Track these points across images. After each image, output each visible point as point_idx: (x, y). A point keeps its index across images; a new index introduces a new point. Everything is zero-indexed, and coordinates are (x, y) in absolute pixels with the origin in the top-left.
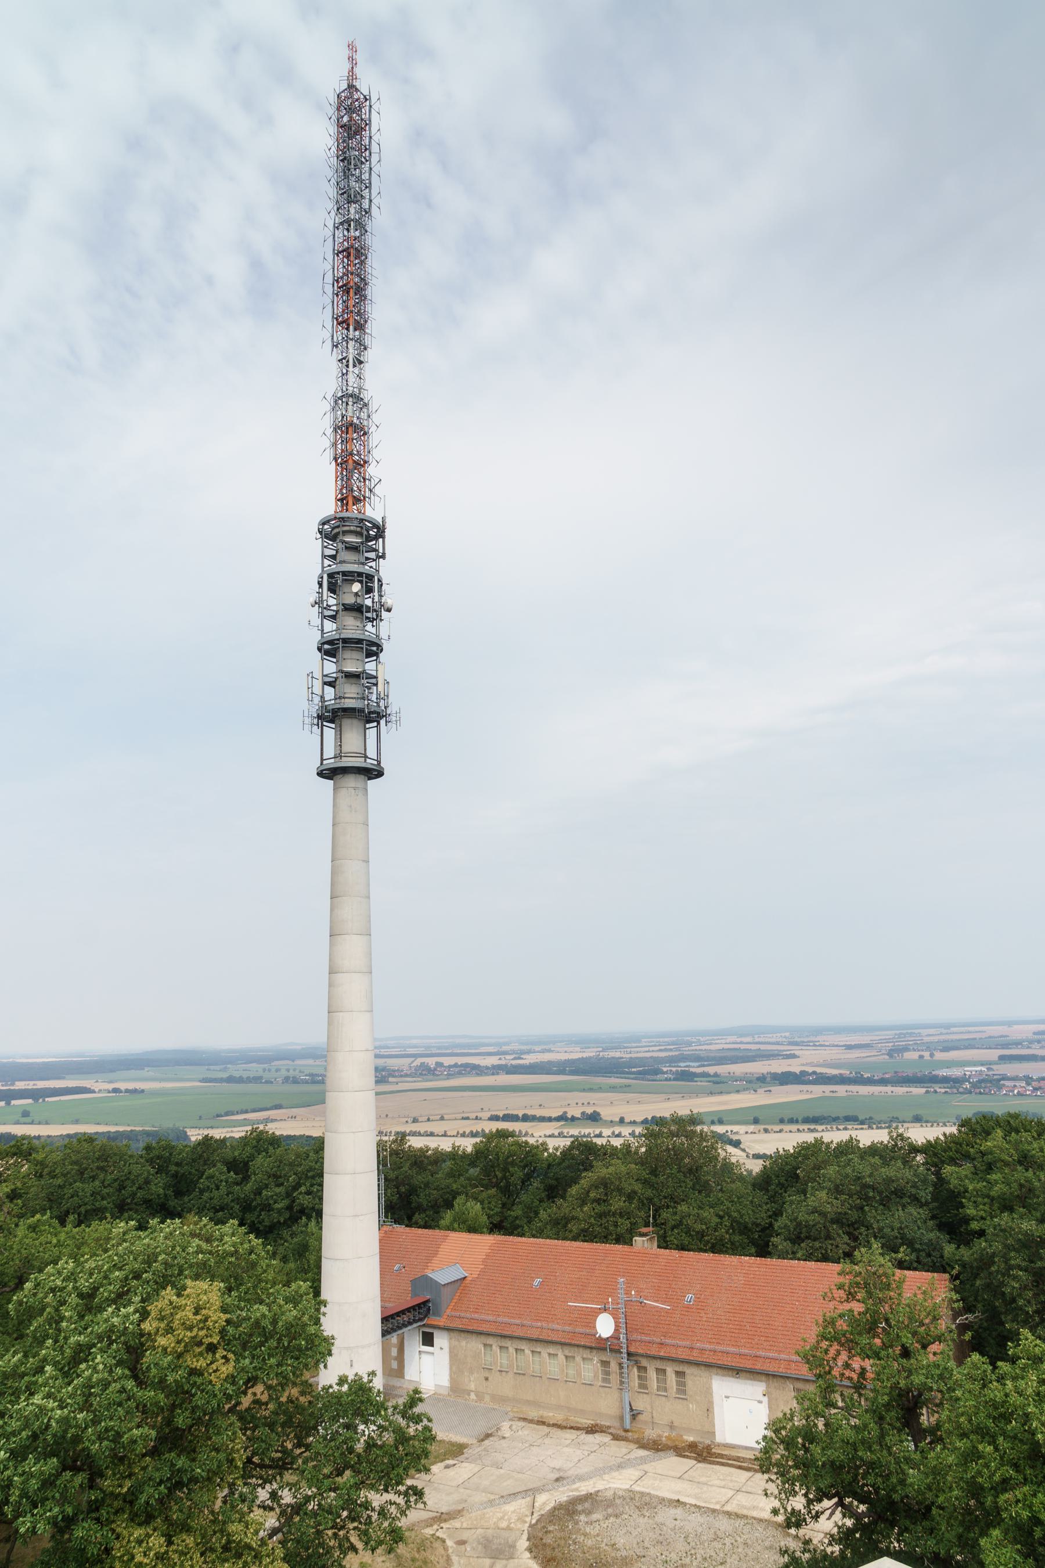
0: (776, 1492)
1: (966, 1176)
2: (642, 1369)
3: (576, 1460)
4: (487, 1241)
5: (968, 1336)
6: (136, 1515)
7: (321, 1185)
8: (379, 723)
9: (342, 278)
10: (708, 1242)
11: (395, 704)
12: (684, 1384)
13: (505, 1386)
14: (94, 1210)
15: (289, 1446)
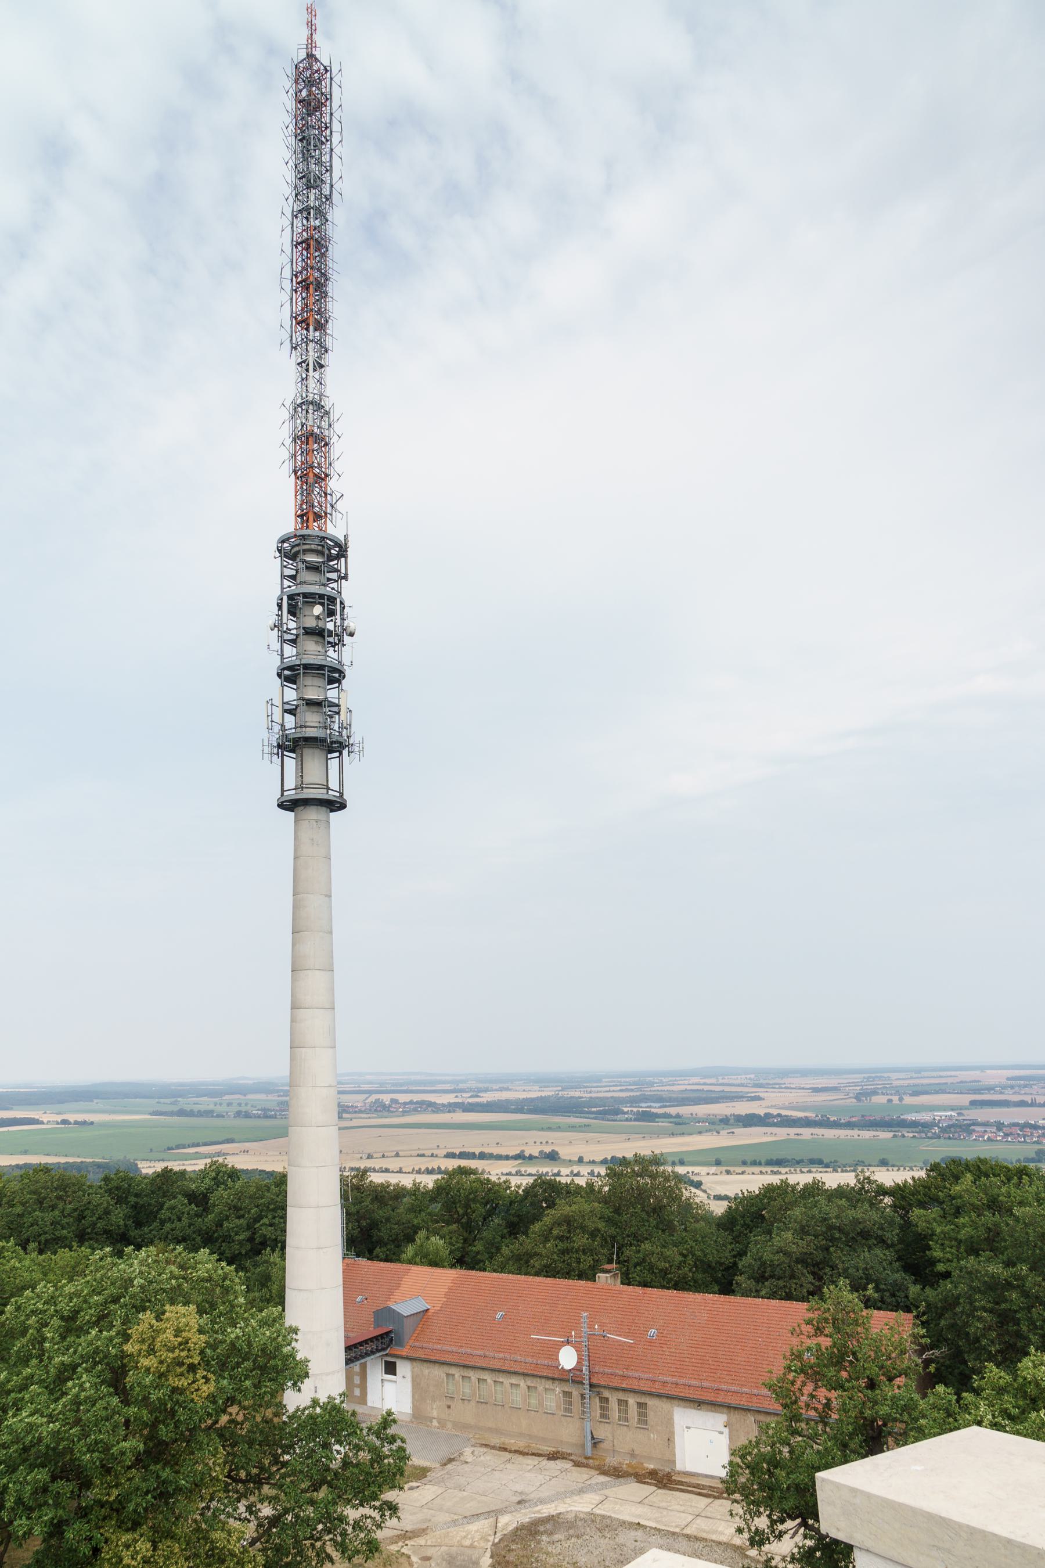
0: (741, 1512)
1: (934, 1219)
2: (604, 1400)
3: (538, 1484)
4: (448, 1276)
5: (932, 1368)
6: (123, 1522)
7: (284, 1217)
8: (341, 753)
9: (301, 272)
10: (671, 1279)
11: (357, 734)
12: (645, 1415)
13: (466, 1413)
14: (54, 1239)
15: (267, 1462)
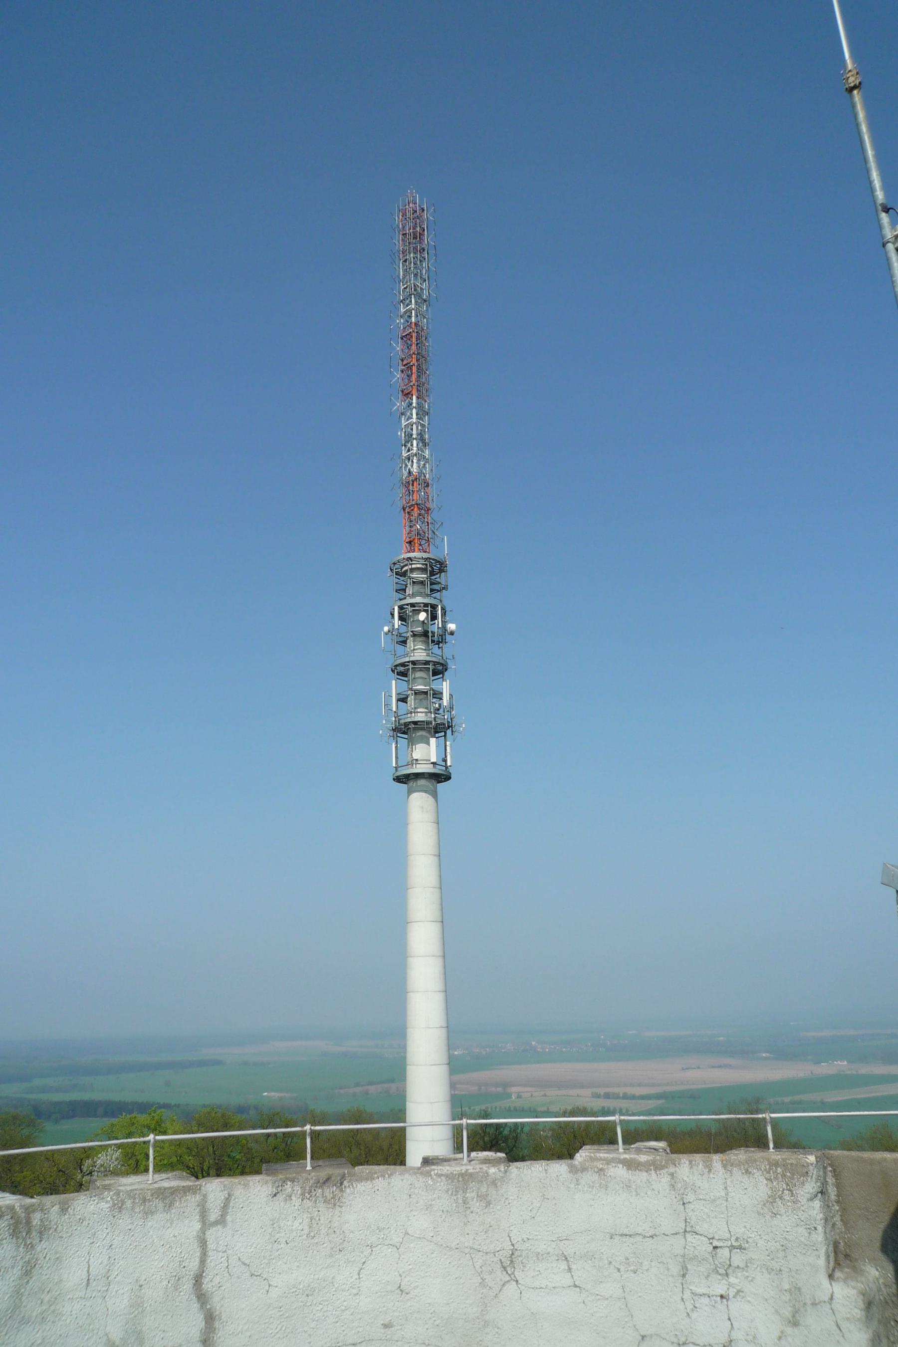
8: (445, 733)
